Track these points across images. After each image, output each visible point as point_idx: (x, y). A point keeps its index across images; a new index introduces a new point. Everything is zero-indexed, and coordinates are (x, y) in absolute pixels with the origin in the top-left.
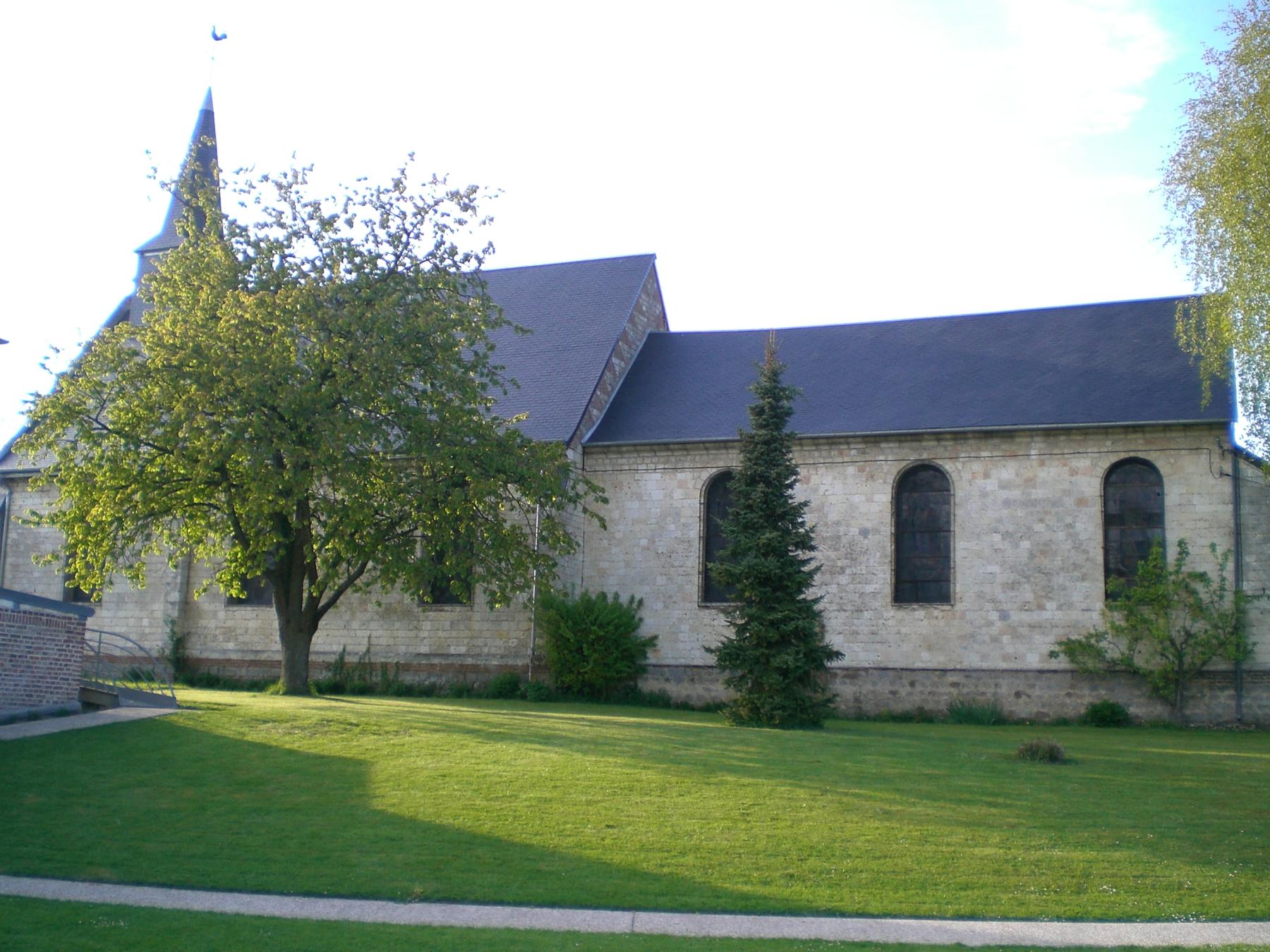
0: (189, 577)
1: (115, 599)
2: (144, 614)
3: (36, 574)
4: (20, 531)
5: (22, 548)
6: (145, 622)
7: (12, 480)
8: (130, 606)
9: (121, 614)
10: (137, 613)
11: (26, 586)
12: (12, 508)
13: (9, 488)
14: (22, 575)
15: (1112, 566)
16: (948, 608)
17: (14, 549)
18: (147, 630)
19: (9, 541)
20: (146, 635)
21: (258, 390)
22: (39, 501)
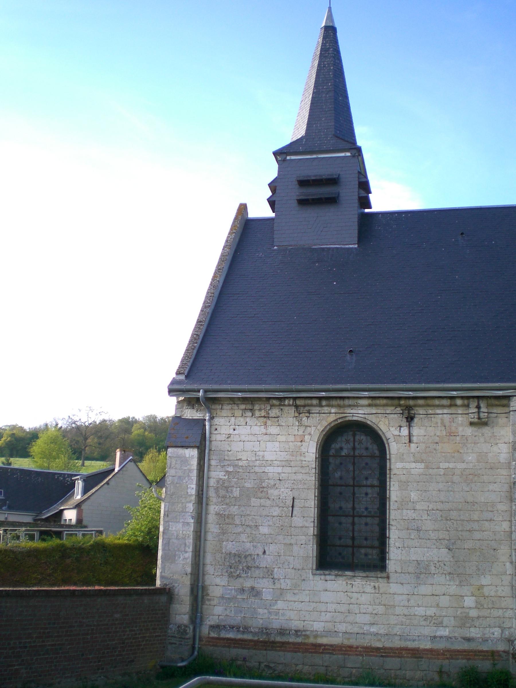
0: (361, 634)
1: (411, 570)
2: (465, 590)
3: (264, 530)
4: (230, 469)
5: (236, 492)
6: (469, 602)
7: (215, 400)
8: (442, 579)
9: (424, 589)
10: (453, 589)
11: (248, 545)
12: (214, 437)
13: (210, 411)
14: (240, 529)
15: (220, 574)
16: (314, 567)
17: (222, 492)
18: (473, 613)
19: (212, 482)
20: (473, 619)
21: (443, 651)
22: (263, 430)
